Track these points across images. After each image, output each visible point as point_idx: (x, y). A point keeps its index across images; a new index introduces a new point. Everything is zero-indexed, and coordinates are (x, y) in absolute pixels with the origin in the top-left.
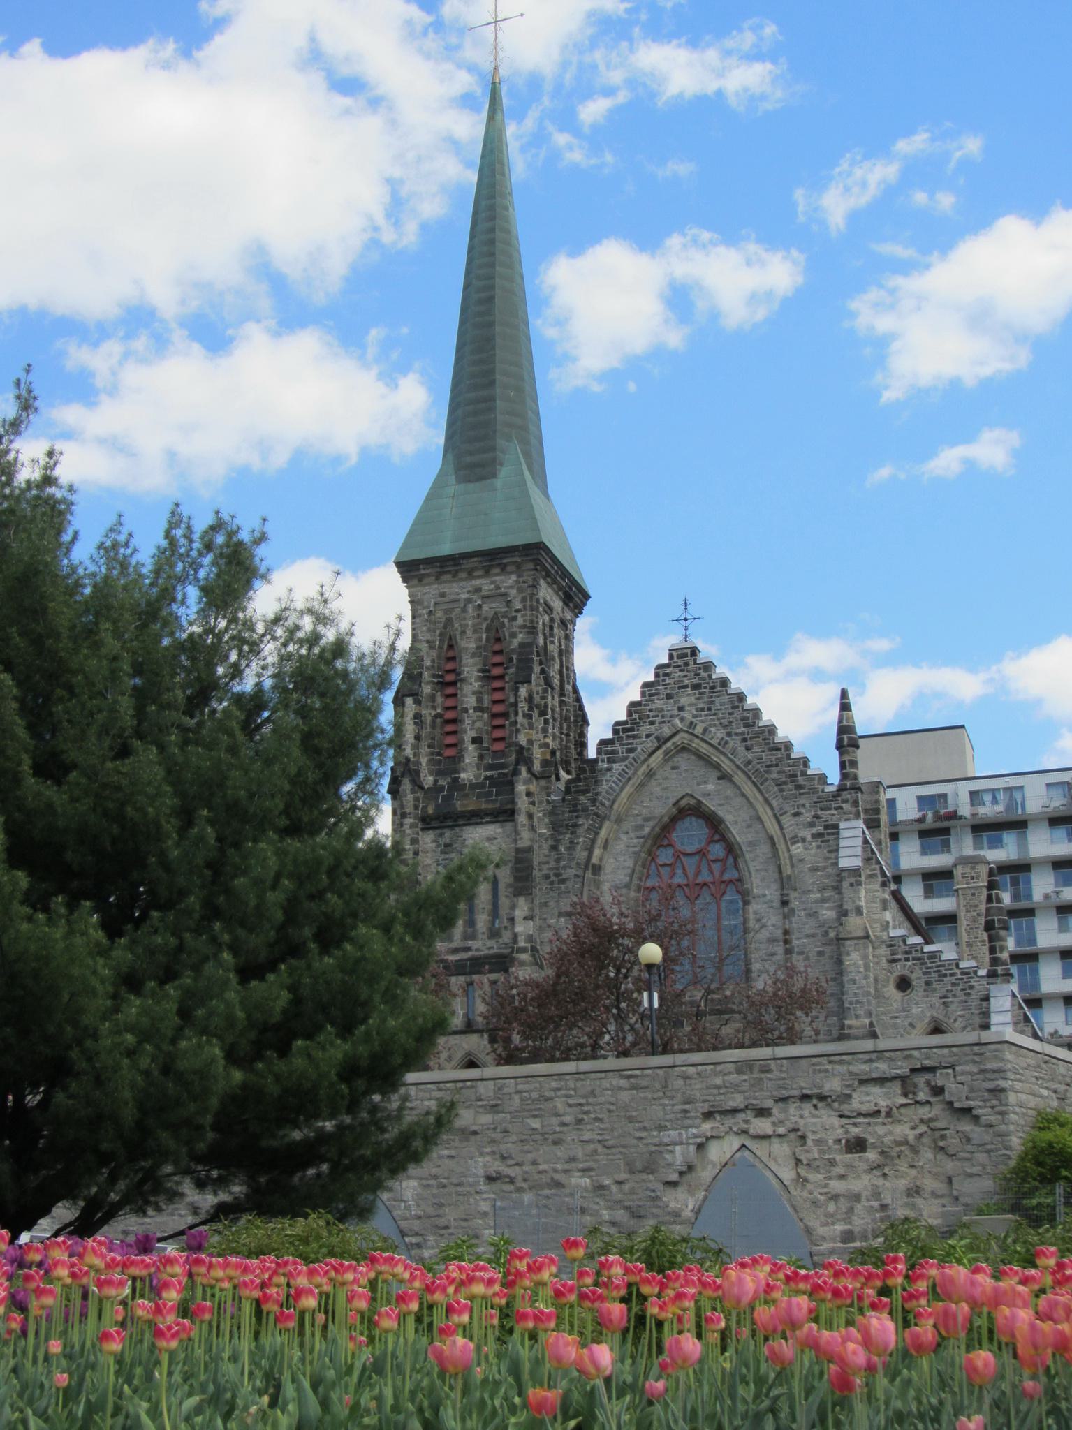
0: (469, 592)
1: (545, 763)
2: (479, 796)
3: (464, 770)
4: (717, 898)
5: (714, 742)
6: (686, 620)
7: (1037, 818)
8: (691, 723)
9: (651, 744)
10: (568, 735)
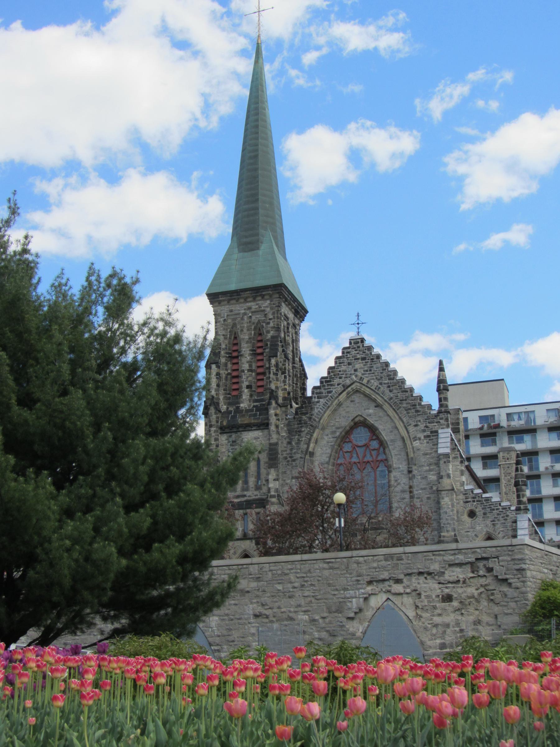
0: (245, 309)
1: (285, 399)
2: (250, 416)
3: (242, 402)
4: (374, 469)
5: (373, 388)
6: (358, 324)
7: (542, 427)
8: (361, 378)
9: (340, 388)
10: (296, 384)
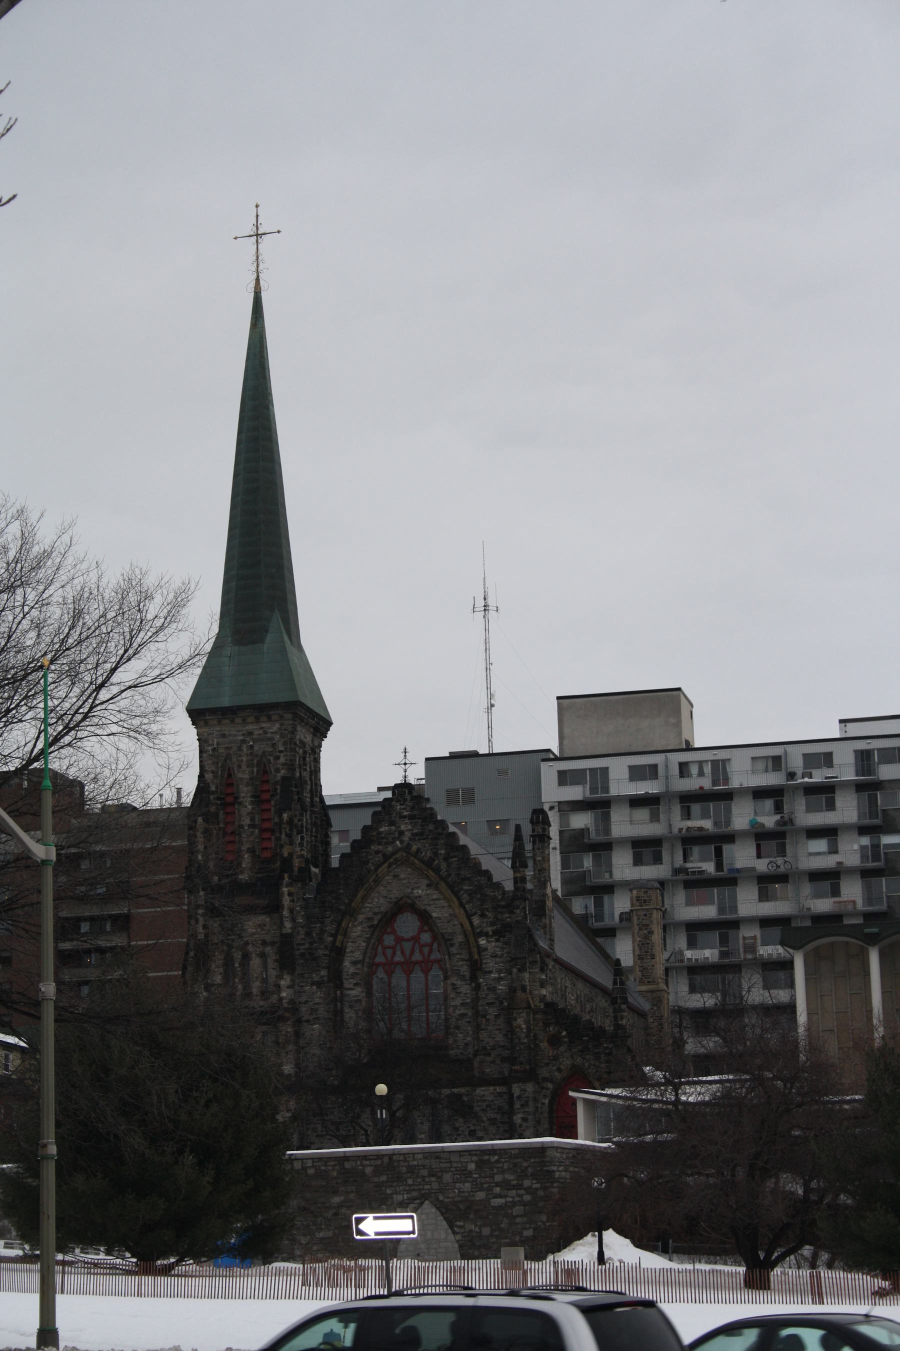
0: (243, 735)
3: (242, 873)
4: (426, 971)
6: (405, 764)
10: (316, 837)
